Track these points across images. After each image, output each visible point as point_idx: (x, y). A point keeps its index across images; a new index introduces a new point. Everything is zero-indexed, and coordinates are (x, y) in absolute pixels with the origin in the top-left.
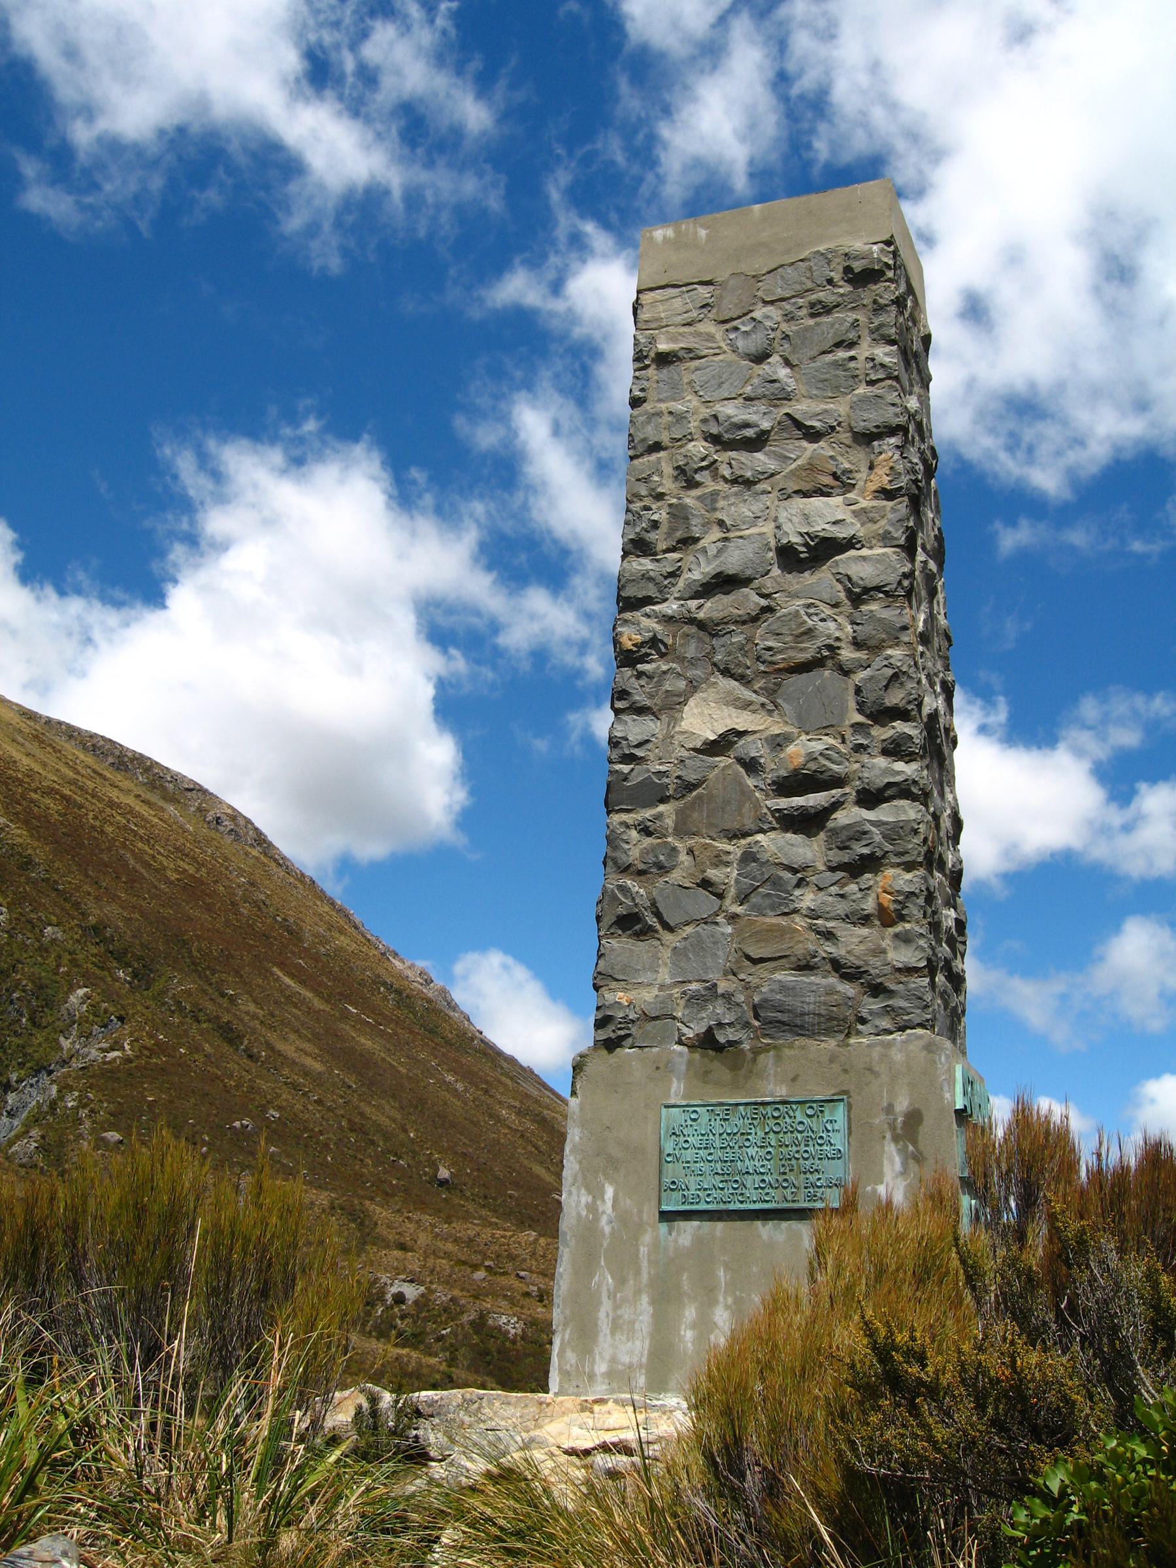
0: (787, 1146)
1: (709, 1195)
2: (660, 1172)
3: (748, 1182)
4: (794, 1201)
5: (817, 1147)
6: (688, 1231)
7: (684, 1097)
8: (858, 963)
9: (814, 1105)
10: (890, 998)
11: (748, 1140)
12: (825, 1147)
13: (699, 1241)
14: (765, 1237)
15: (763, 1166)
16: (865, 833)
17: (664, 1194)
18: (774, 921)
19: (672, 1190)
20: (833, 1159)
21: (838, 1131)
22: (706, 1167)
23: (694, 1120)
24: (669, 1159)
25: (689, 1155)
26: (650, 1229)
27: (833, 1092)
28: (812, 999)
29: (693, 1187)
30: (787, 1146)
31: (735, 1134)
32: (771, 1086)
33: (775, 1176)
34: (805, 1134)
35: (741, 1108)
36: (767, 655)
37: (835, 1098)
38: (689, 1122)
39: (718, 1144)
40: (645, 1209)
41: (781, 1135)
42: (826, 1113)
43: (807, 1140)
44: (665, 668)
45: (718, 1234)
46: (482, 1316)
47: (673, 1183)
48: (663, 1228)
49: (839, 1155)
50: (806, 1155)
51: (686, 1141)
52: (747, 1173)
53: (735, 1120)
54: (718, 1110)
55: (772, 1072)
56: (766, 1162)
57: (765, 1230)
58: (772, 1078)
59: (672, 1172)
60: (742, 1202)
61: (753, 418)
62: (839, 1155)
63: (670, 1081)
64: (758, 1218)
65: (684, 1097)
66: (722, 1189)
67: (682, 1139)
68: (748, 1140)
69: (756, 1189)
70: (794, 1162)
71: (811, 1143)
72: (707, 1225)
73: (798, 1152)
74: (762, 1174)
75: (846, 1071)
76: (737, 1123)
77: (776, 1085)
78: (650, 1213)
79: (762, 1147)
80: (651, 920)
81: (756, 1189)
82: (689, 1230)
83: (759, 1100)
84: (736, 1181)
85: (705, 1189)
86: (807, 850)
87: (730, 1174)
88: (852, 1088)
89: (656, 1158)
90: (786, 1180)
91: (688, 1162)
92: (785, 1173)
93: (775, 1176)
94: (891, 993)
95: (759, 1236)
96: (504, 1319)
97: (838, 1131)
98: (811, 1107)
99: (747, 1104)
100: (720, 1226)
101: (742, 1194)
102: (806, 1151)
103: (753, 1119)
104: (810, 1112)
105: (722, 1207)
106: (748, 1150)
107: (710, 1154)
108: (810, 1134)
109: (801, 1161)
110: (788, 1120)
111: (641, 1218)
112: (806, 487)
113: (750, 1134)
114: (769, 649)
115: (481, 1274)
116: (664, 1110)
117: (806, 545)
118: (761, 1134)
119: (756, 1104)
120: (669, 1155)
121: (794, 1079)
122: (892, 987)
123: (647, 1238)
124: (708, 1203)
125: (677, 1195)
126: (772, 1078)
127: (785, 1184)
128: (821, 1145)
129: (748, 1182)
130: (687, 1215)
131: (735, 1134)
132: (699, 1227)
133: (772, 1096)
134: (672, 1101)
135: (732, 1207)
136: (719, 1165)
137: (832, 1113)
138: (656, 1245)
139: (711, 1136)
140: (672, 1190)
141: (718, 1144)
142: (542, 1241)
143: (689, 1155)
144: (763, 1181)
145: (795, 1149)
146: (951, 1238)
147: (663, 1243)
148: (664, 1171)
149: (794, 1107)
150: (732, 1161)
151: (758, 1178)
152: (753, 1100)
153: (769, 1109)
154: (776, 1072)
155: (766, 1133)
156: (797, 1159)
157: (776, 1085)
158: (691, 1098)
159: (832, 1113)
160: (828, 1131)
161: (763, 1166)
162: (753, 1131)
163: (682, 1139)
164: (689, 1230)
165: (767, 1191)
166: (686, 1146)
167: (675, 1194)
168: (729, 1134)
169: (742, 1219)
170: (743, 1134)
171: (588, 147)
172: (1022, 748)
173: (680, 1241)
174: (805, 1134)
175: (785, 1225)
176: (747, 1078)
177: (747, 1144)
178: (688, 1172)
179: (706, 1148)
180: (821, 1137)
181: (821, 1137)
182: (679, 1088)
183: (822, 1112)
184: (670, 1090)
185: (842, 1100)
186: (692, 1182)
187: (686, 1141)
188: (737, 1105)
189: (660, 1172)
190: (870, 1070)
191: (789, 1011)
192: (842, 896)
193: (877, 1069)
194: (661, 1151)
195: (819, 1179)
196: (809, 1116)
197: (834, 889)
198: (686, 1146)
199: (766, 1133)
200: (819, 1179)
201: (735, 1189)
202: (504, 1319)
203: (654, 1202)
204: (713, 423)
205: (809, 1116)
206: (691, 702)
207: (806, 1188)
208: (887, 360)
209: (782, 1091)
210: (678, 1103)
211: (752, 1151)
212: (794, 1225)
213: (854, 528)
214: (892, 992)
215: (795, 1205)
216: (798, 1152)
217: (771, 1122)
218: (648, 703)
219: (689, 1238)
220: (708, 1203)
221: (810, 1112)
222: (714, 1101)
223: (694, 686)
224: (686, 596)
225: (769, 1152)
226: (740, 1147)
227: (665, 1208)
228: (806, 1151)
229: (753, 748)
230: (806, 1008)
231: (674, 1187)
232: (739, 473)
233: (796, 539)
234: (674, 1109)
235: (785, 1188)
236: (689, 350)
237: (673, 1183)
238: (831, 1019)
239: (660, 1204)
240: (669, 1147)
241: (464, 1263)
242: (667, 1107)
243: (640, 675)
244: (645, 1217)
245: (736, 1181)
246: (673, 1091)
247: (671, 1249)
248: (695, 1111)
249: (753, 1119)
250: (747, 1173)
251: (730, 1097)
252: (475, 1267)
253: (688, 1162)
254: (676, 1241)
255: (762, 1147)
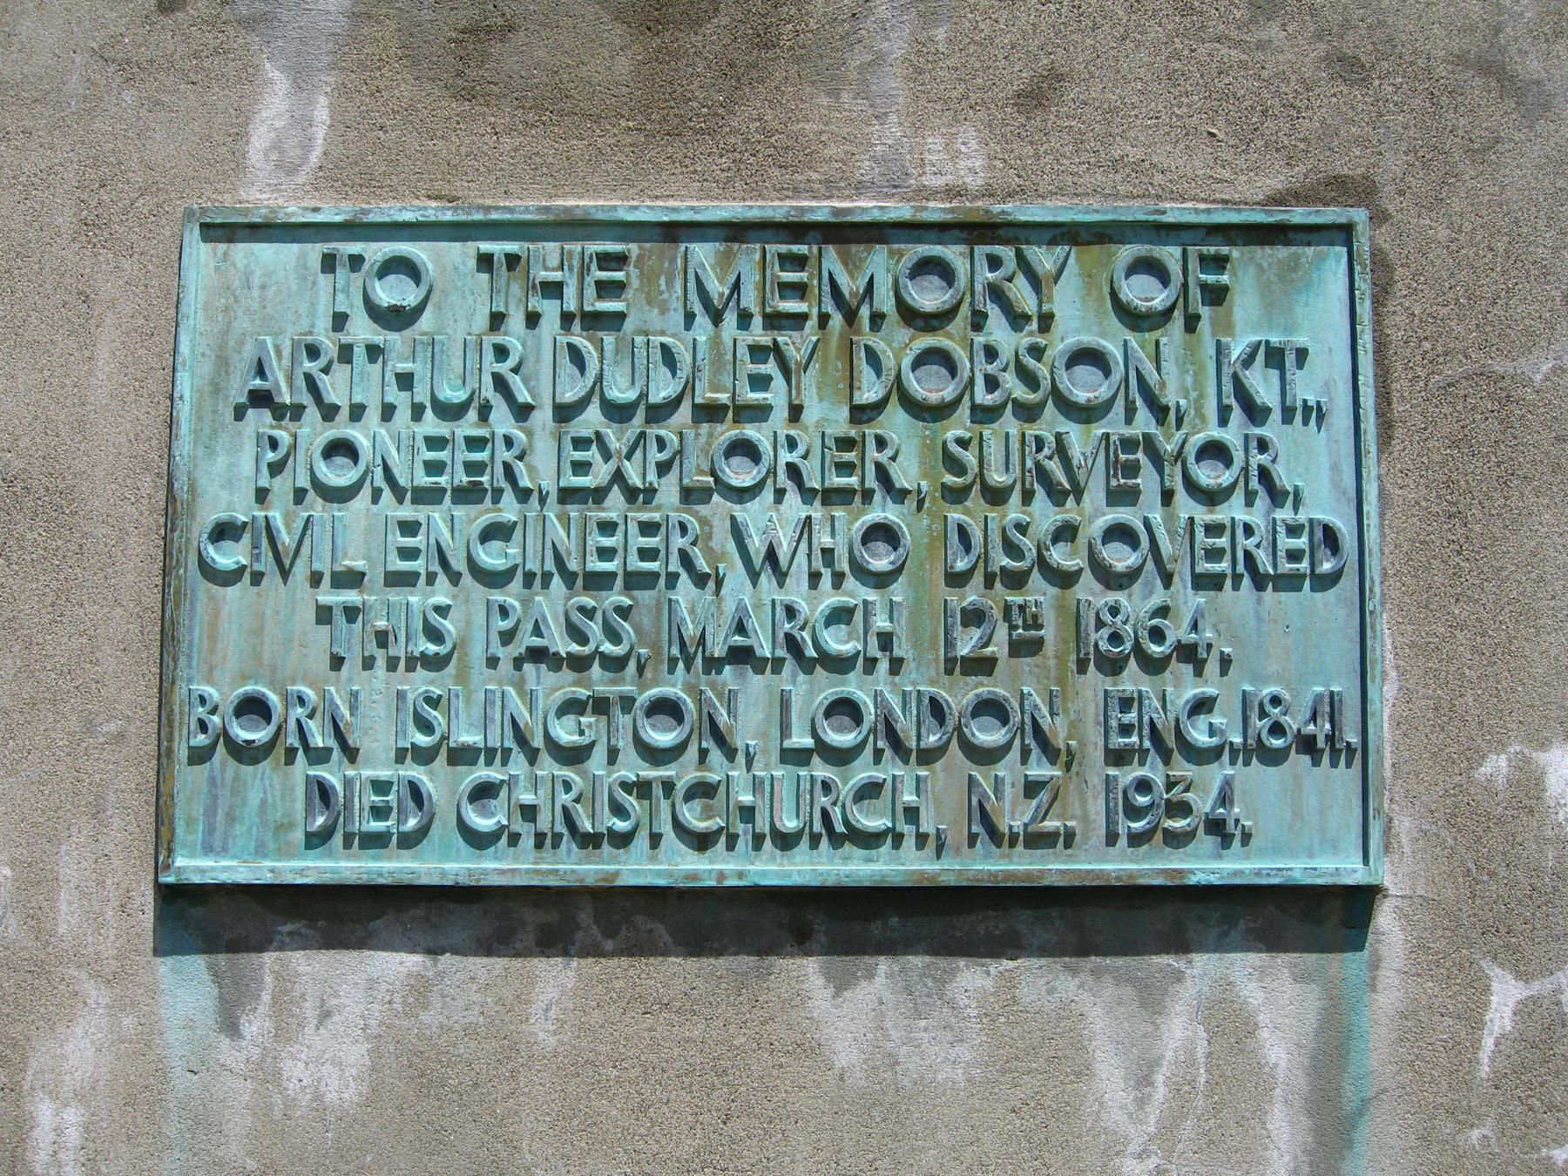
0: (996, 496)
1: (483, 792)
2: (168, 638)
3: (750, 705)
4: (1038, 840)
5: (1186, 507)
6: (344, 1011)
7: (331, 177)
9: (1170, 255)
11: (747, 449)
12: (1234, 511)
13: (417, 1074)
14: (846, 1054)
15: (840, 615)
17: (189, 780)
19: (245, 754)
20: (1289, 583)
21: (1316, 414)
22: (468, 614)
23: (396, 318)
24: (226, 557)
25: (359, 532)
26: (97, 995)
27: (1275, 181)
29: (379, 735)
30: (996, 496)
31: (659, 413)
32: (893, 130)
33: (922, 679)
34: (1113, 425)
35: (703, 253)
37: (1298, 215)
38: (362, 330)
39: (544, 468)
40: (71, 866)
41: (956, 428)
42: (1245, 303)
43: (1123, 462)
45: (543, 1033)
47: (253, 707)
48: (187, 985)
49: (1323, 558)
50: (1120, 558)
51: (341, 449)
52: (742, 656)
53: (655, 318)
54: (547, 258)
55: (897, 47)
56: (856, 593)
57: (848, 1011)
58: (893, 83)
59: (250, 638)
60: (702, 842)
62: (1323, 558)
63: (249, 75)
64: (801, 940)
65: (331, 177)
66: (574, 756)
67: (313, 432)
68: (747, 449)
69: (797, 757)
70: (1040, 593)
71: (1148, 481)
72: (470, 980)
73: (1066, 533)
74: (838, 664)
75: (1349, 68)
76: (673, 335)
77: (919, 126)
78: (99, 895)
79: (831, 496)
81: (797, 757)
82: (352, 1003)
83: (821, 209)
84: (666, 708)
85: (462, 756)
87: (629, 657)
88: (1393, 164)
89: (140, 549)
90: (991, 708)
91: (352, 579)
92: (981, 665)
93: (922, 679)
95: (810, 1050)
97: (1316, 414)
98: (1155, 269)
99: (735, 232)
100: (554, 982)
101: (703, 791)
102: (1121, 533)
103: (775, 321)
104: (1144, 293)
105: (573, 867)
106: (753, 514)
107: (495, 532)
108: (1144, 422)
109: (1088, 590)
110: (998, 331)
111: (38, 920)
113: (760, 412)
116: (201, 255)
118: (826, 415)
119: (796, 230)
120: (224, 532)
121: (1033, 98)
123: (79, 1048)
124: (478, 841)
125: (278, 789)
126: (893, 83)
127: (987, 735)
128: (1212, 497)
129: (750, 705)
130: (342, 915)
131: (659, 413)
132: (419, 989)
133: (895, 187)
134: (259, 197)
135: (636, 868)
136: (553, 603)
137: (1275, 304)
138: (137, 1095)
139: (502, 421)
140: (245, 754)
141: (544, 468)
143: (359, 532)
144: (845, 709)
145: (1045, 515)
146: (1398, 433)
147: (181, 1081)
148: (194, 634)
149: (1044, 258)
150: (636, 581)
151: (811, 693)
152: (777, 208)
153: (880, 264)
154: (920, 45)
155: (861, 413)
156: (1065, 579)
157: (919, 126)
158: (370, 184)
159: (1275, 304)
160: (1255, 412)
161: (840, 615)
162: (776, 396)
163: (313, 432)
164: (352, 1003)
165: (863, 771)
166: (338, 475)
167: (261, 780)
168: (618, 412)
169: (696, 943)
170: (709, 413)
171: (1225, 250)
173: (295, 1071)
174: (1113, 425)
175: (973, 979)
176: (735, 76)
177: (740, 474)
178: (354, 641)
179: (468, 494)
180: (1215, 451)
181: (1215, 451)
182: (303, 122)
183: (1216, 295)
184: (240, 135)
185: (1345, 232)
186: (377, 707)
187: (341, 449)
188: (673, 232)
189: (168, 638)
190: (1494, 69)
193: (1532, 67)
194: (173, 508)
195: (1202, 706)
196: (1133, 318)
198: (338, 475)
199: (861, 413)
200: (1202, 706)
201: (655, 755)
203: (128, 825)
205: (1133, 318)
207: (1118, 757)
209: (957, 163)
210: (295, 212)
211: (773, 520)
212: (1040, 982)
215: (1052, 867)
216: (1066, 533)
217: (898, 346)
219: (357, 1054)
220: (478, 841)
221: (1144, 293)
222: (526, 205)
225: (883, 533)
226: (690, 495)
227: (195, 865)
228: (1121, 533)
231: (259, 731)
234: (266, 252)
235: (986, 756)
237: (253, 707)
239: (163, 843)
240: (225, 479)
242: (221, 232)
244: (67, 917)
245: (666, 708)
246: (259, 140)
247: (238, 1123)
248: (407, 268)
249: (775, 321)
250: (742, 656)
251: (624, 184)
253: (352, 579)
254: (266, 1073)
255: (831, 496)
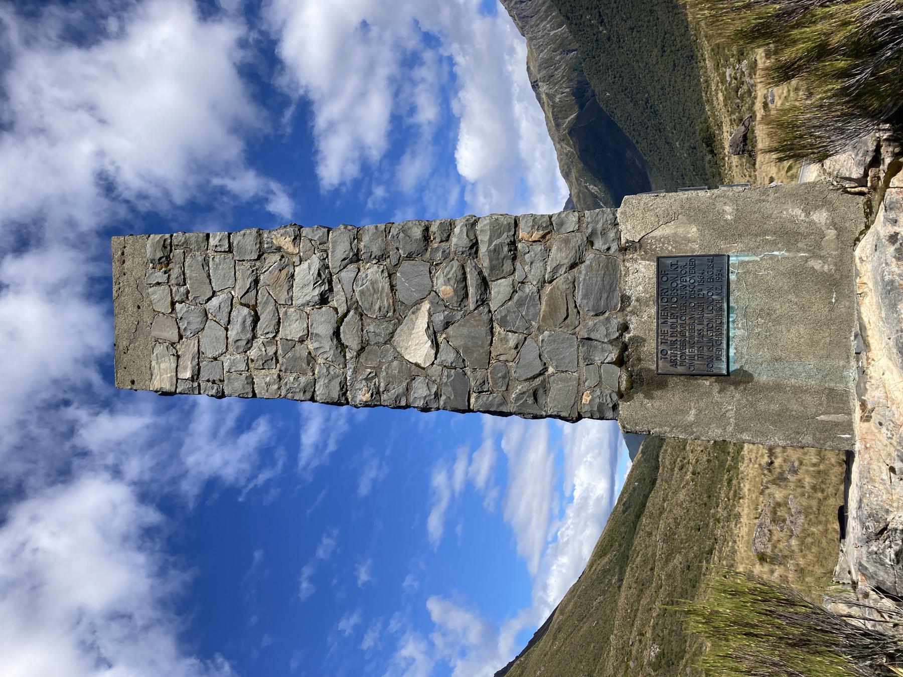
8: (574, 251)
10: (596, 233)
16: (495, 250)
18: (544, 303)
28: (595, 279)
36: (384, 311)
44: (384, 374)
46: (650, 664)
61: (240, 320)
80: (538, 381)
86: (500, 289)
94: (593, 233)
96: (652, 653)
112: (286, 287)
114: (380, 309)
115: (631, 664)
117: (321, 285)
122: (590, 230)
142: (615, 632)
172: (459, 143)
191: (601, 293)
192: (532, 263)
197: (527, 268)
202: (652, 653)
204: (239, 343)
206: (407, 357)
208: (218, 238)
213: (315, 262)
214: (592, 233)
218: (405, 384)
223: (399, 357)
224: (343, 360)
229: (439, 318)
230: (600, 283)
232: (272, 327)
233: (317, 291)
236: (193, 358)
238: (607, 267)
241: (626, 672)
243: (386, 390)
252: (627, 667)
